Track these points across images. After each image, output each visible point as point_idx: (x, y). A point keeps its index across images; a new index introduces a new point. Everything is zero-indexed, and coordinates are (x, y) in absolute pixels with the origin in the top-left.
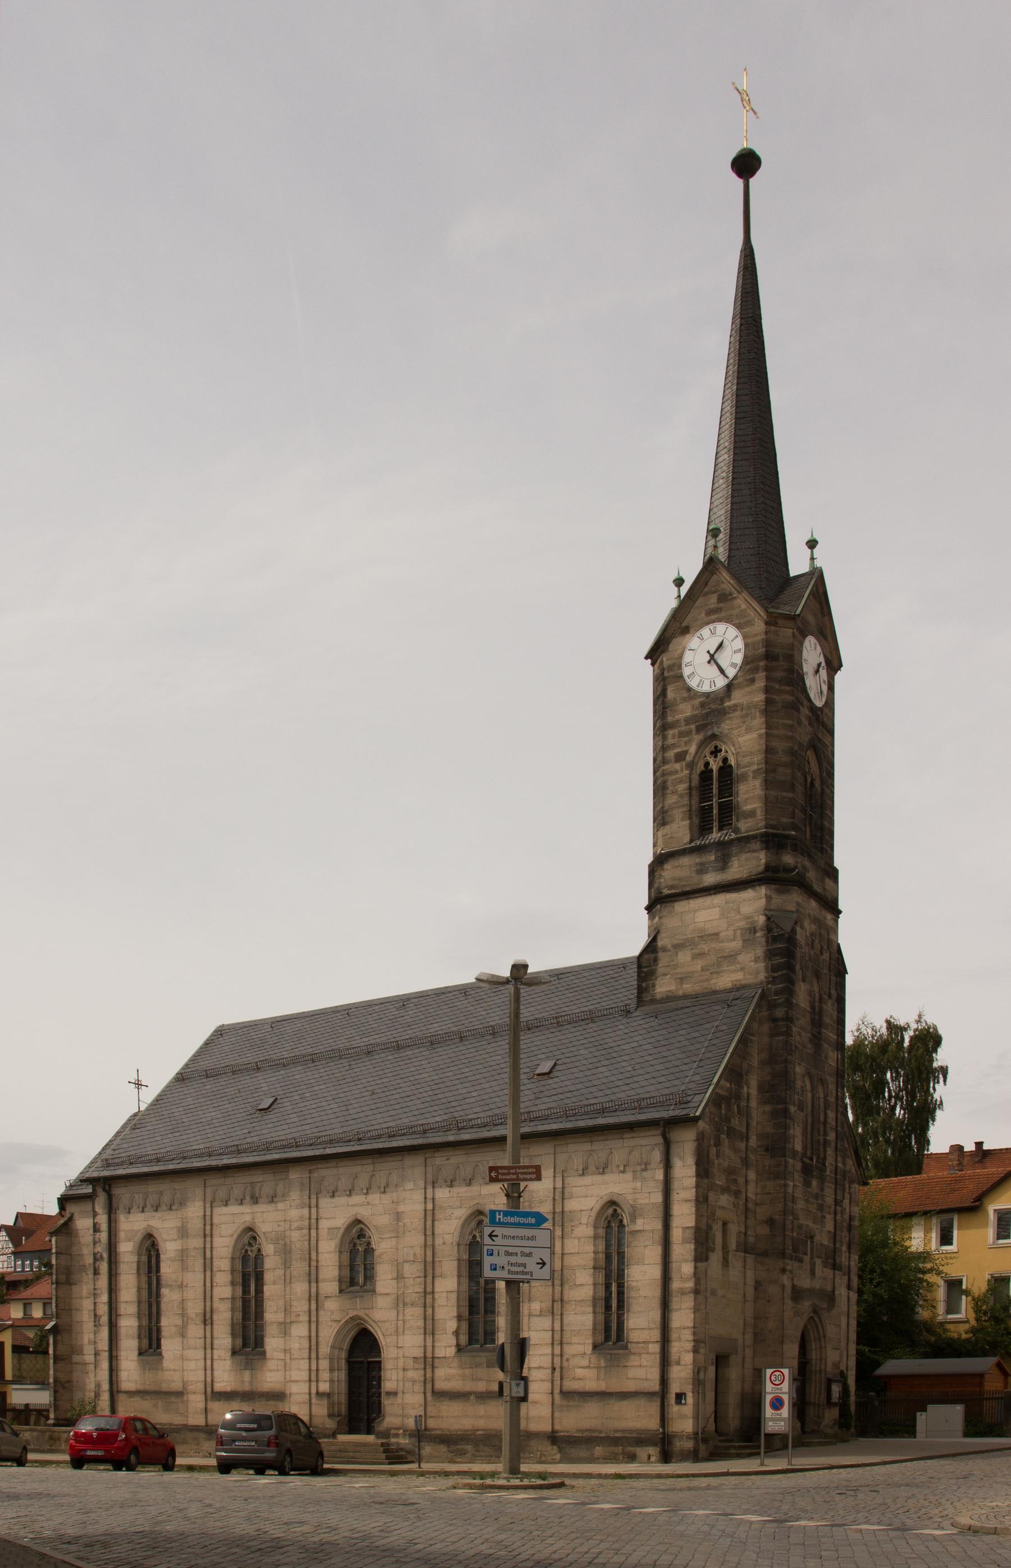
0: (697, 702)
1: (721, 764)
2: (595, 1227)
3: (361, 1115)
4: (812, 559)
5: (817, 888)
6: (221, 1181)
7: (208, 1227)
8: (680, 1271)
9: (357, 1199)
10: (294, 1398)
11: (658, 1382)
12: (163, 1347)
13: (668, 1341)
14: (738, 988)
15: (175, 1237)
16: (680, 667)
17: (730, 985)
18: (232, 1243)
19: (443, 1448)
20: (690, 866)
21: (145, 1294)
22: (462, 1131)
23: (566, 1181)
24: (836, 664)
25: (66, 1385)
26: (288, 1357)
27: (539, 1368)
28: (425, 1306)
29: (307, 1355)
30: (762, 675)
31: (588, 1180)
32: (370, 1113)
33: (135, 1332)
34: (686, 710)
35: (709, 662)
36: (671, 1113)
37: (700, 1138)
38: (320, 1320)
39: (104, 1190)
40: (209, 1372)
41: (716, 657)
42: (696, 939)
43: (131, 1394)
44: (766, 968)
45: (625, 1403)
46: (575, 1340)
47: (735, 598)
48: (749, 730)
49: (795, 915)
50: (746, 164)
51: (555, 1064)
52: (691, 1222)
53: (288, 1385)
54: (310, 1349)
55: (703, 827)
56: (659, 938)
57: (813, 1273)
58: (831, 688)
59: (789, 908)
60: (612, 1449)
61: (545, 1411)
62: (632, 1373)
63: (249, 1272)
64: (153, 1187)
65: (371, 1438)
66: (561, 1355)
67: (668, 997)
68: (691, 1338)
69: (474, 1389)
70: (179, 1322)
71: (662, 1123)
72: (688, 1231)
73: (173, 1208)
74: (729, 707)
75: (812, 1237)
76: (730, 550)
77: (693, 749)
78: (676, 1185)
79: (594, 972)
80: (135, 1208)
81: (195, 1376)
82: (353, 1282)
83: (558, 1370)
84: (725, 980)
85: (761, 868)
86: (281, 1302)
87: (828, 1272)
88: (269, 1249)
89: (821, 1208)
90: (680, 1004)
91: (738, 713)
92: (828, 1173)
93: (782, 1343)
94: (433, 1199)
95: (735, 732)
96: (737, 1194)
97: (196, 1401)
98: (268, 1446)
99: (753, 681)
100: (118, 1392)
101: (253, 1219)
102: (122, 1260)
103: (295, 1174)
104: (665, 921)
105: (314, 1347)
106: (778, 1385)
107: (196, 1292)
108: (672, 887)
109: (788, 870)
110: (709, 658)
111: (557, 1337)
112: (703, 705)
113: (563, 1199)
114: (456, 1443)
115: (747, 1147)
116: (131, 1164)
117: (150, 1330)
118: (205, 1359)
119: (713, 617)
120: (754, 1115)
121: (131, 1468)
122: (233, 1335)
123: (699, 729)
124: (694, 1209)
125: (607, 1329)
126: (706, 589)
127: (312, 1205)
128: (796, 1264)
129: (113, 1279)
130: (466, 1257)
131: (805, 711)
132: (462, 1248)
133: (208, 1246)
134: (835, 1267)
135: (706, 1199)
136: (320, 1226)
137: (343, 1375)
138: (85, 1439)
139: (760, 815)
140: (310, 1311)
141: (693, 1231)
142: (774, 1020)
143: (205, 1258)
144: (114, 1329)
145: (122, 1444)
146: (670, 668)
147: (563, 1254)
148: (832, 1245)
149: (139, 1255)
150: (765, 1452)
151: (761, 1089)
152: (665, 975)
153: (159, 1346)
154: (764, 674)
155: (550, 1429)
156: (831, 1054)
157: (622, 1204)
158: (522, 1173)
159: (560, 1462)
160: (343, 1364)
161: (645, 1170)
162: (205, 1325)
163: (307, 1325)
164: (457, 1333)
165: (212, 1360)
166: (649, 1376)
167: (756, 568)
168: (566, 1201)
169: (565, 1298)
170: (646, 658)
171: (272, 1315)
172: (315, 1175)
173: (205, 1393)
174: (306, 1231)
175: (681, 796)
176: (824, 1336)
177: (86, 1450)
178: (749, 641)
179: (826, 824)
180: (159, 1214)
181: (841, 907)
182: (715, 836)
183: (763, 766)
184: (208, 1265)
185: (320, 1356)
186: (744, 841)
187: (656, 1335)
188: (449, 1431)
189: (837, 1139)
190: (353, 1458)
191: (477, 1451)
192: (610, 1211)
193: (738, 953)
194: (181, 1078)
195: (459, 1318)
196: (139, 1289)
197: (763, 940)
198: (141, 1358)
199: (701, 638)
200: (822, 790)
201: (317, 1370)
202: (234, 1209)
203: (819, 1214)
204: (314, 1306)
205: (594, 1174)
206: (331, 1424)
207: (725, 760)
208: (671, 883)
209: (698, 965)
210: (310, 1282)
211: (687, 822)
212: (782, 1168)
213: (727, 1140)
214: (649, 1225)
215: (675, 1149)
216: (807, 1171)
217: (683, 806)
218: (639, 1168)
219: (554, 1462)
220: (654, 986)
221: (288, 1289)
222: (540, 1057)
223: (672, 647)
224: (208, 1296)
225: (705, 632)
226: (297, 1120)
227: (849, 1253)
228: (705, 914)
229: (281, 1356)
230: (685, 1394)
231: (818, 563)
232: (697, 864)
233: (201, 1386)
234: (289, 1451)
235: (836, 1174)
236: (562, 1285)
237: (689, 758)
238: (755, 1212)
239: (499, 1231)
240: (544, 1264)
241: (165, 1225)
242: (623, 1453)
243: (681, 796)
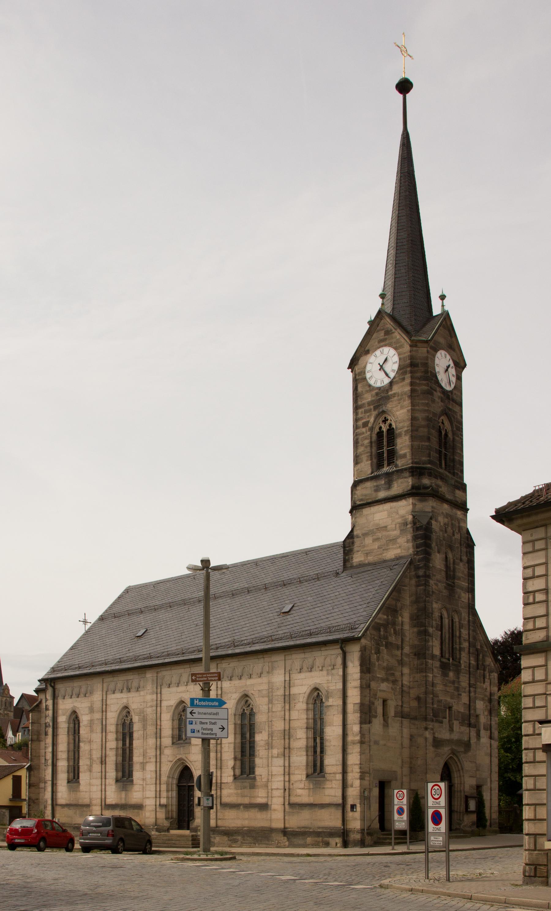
0: (374, 393)
1: (388, 427)
2: (307, 704)
3: (188, 639)
4: (443, 306)
5: (448, 496)
6: (111, 679)
7: (104, 706)
8: (352, 730)
9: (182, 688)
10: (148, 808)
11: (341, 798)
12: (80, 778)
13: (346, 773)
14: (398, 558)
15: (87, 713)
16: (365, 373)
17: (393, 557)
18: (117, 716)
19: (226, 838)
20: (371, 487)
21: (72, 746)
22: (237, 648)
23: (291, 676)
24: (462, 364)
25: (36, 801)
26: (145, 784)
27: (277, 789)
28: (217, 752)
29: (154, 782)
30: (408, 376)
31: (302, 675)
32: (192, 637)
33: (65, 769)
34: (368, 398)
35: (380, 370)
36: (346, 635)
37: (363, 650)
38: (162, 761)
39: (51, 686)
40: (103, 792)
41: (384, 366)
42: (375, 530)
43: (63, 806)
44: (413, 546)
45: (323, 810)
46: (296, 772)
47: (394, 332)
48: (402, 408)
49: (431, 514)
50: (404, 87)
51: (293, 606)
52: (358, 700)
53: (145, 800)
54: (156, 778)
55: (380, 465)
56: (355, 530)
57: (451, 730)
58: (459, 378)
59: (427, 510)
60: (316, 839)
61: (280, 815)
62: (327, 792)
63: (126, 733)
64: (76, 684)
65: (187, 832)
66: (289, 781)
67: (360, 565)
68: (359, 770)
69: (243, 802)
70: (89, 763)
71: (340, 641)
72: (356, 706)
73: (87, 695)
74: (391, 395)
75: (450, 708)
76: (394, 305)
77: (372, 420)
78: (349, 678)
79: (326, 550)
80: (67, 696)
81: (96, 795)
82: (180, 738)
83: (287, 791)
84: (391, 554)
85: (410, 487)
86: (142, 750)
87: (465, 729)
88: (135, 719)
89: (457, 689)
90: (366, 568)
91: (396, 398)
92: (463, 667)
93: (426, 773)
94: (221, 688)
95: (394, 409)
96: (394, 682)
97: (97, 809)
98: (108, 836)
99: (403, 379)
100: (56, 805)
101: (128, 701)
102: (60, 727)
103: (150, 675)
104: (358, 520)
105: (158, 777)
106: (436, 799)
107: (98, 744)
108: (361, 500)
109: (426, 488)
110: (379, 368)
111: (287, 770)
112: (377, 394)
113: (290, 687)
114: (232, 835)
115: (402, 654)
116: (66, 670)
117: (74, 768)
118: (102, 785)
119: (382, 344)
120: (407, 634)
121: (40, 850)
122: (117, 770)
123: (375, 408)
124: (359, 692)
125: (315, 765)
126: (378, 328)
127: (158, 692)
128: (436, 725)
129: (55, 738)
130: (239, 722)
131: (438, 394)
132: (237, 717)
133: (104, 718)
134: (470, 725)
135: (369, 686)
136: (162, 705)
137: (175, 794)
138: (14, 832)
139: (409, 456)
140: (156, 755)
141: (358, 706)
142: (418, 577)
143: (102, 725)
144: (55, 767)
145: (35, 835)
146: (360, 374)
147: (290, 720)
148: (468, 712)
149: (69, 723)
150: (410, 842)
151: (411, 618)
152: (358, 551)
153: (78, 778)
154: (410, 375)
155: (283, 826)
156: (463, 595)
157: (321, 690)
158: (210, 677)
159: (288, 847)
160: (175, 787)
161: (333, 669)
162: (102, 764)
163: (155, 764)
164: (234, 768)
165: (105, 785)
166: (337, 794)
167: (412, 314)
168: (291, 688)
169: (291, 746)
170: (348, 368)
171: (137, 758)
172: (160, 675)
173: (101, 805)
174: (154, 708)
175: (366, 447)
176: (462, 769)
177: (15, 839)
178: (401, 356)
179: (457, 458)
180: (79, 699)
181: (468, 506)
182: (386, 469)
183: (410, 428)
184: (104, 729)
185: (162, 783)
186: (400, 472)
187: (340, 769)
188: (229, 828)
189: (469, 646)
190: (174, 844)
191: (244, 840)
192: (316, 694)
193: (398, 537)
194: (102, 619)
195: (235, 759)
196: (69, 744)
197: (411, 530)
198: (69, 784)
199: (376, 356)
200: (453, 438)
201: (160, 791)
202: (118, 695)
203: (456, 693)
204: (158, 753)
205: (306, 672)
206: (167, 824)
207: (390, 425)
208: (361, 498)
209: (376, 545)
210: (156, 738)
211: (370, 462)
212: (424, 665)
213: (385, 651)
214: (335, 702)
215: (349, 657)
216: (444, 667)
217: (367, 453)
218: (330, 668)
219: (285, 847)
220: (352, 558)
221: (145, 742)
222: (286, 602)
223: (360, 362)
224: (103, 747)
225: (378, 352)
226: (154, 642)
227: (491, 716)
228: (379, 515)
229: (141, 782)
230: (356, 805)
231: (446, 308)
232: (375, 486)
233: (99, 801)
234: (122, 840)
235: (469, 668)
236: (289, 739)
237: (370, 425)
238: (409, 693)
239: (196, 710)
240: (223, 729)
241: (82, 705)
242: (322, 841)
243: (366, 447)
